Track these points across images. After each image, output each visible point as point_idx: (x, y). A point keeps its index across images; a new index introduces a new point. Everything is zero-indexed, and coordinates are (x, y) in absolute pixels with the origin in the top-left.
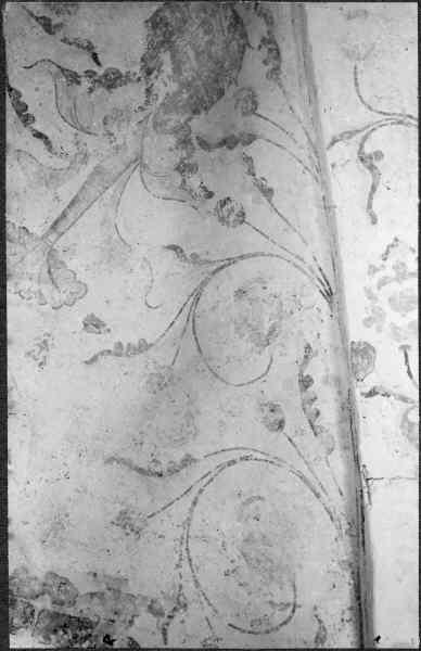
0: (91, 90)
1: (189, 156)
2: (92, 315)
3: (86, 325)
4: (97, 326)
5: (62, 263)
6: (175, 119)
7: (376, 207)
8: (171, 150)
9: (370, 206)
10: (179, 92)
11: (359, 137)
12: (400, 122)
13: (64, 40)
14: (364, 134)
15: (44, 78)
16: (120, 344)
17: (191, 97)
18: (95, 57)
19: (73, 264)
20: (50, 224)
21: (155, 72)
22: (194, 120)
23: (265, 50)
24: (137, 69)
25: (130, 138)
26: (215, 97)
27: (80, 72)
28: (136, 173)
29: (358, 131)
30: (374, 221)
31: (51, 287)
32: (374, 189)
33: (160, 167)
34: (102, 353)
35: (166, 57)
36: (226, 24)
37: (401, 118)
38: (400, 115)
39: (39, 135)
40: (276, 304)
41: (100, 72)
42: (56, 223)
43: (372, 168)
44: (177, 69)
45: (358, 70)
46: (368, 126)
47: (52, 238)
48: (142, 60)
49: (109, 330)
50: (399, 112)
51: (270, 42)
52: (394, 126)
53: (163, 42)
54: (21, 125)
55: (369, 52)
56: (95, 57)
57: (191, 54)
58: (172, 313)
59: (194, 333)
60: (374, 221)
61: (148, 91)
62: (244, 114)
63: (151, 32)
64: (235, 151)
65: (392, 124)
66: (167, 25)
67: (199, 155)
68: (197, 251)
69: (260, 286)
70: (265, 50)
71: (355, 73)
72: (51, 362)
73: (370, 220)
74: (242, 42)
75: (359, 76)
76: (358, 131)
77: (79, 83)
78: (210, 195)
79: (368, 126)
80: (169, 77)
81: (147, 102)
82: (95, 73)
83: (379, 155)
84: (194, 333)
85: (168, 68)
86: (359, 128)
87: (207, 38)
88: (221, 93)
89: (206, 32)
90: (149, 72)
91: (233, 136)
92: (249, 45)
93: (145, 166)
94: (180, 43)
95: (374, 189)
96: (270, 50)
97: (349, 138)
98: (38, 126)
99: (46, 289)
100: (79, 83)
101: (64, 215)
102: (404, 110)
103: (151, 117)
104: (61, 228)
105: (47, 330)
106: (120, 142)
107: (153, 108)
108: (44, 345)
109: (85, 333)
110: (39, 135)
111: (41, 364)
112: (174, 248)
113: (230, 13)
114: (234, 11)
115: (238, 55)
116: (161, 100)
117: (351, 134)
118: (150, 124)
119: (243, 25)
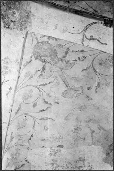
0: (44, 72)
1: (66, 61)
2: (87, 88)
3: (89, 89)
4: (90, 88)
5: (74, 88)
6: (56, 60)
7: (103, 43)
8: (62, 63)
9: (102, 43)
10: (51, 57)
11: (85, 38)
12: (87, 29)
13: (34, 75)
14: (84, 37)
15: (84, 146)
16: (96, 86)
17: (53, 55)
18: (39, 70)
19: (75, 86)
20: (66, 87)
21: (45, 61)
22: (58, 57)
23: (50, 39)
24: (43, 63)
25: (56, 68)
26: (56, 51)
27: (40, 73)
28: (64, 70)
29: (83, 38)
30: (106, 44)
31: (78, 91)
32: (99, 41)
33: (65, 66)
34: (96, 90)
35: (43, 58)
36: (42, 45)
37: (86, 28)
38: (85, 28)
39: (49, 83)
40: (108, 60)
41: (42, 70)
42: (66, 86)
43: (93, 39)
44: (46, 56)
45: (69, 32)
46: (83, 35)
47: (69, 87)
48: (42, 62)
49: (92, 87)
50: (84, 28)
51: (49, 38)
52: (87, 31)
53: (40, 58)
54: (46, 86)
55: (66, 28)
56: (39, 70)
57: (44, 53)
58: (96, 76)
59: (103, 75)
60: (106, 44)
61: (48, 63)
62: (62, 48)
63: (38, 59)
64: (69, 53)
65: (86, 30)
66: (37, 56)
67: (66, 59)
68: (87, 67)
69: (102, 61)
70: (50, 39)
71: (69, 32)
72: (92, 97)
73: (105, 45)
74: (46, 43)
75: (70, 32)
76: (83, 38)
77: (42, 74)
78: (76, 60)
79: (83, 35)
80: (47, 58)
81: (50, 63)
82: (42, 71)
83: (91, 36)
84: (103, 75)
85: (45, 58)
86: (83, 37)
87: (43, 49)
88: (55, 50)
89: (42, 49)
90: (45, 61)
91: (66, 52)
92: (47, 42)
93: (63, 68)
94: (42, 54)
95: (99, 41)
96: (51, 38)
97: (84, 40)
98: (48, 83)
99: (78, 92)
100: (42, 74)
101: (66, 84)
102: (84, 27)
103: (54, 64)
104: (68, 85)
105: (86, 95)
106: (56, 70)
107: (52, 63)
108: (88, 97)
109: (90, 90)
110: (49, 83)
111: (92, 99)
112: (83, 70)
113: (40, 43)
114: (40, 42)
115: (49, 44)
116: (51, 61)
117: (83, 39)
118: (55, 64)
119: (43, 42)
